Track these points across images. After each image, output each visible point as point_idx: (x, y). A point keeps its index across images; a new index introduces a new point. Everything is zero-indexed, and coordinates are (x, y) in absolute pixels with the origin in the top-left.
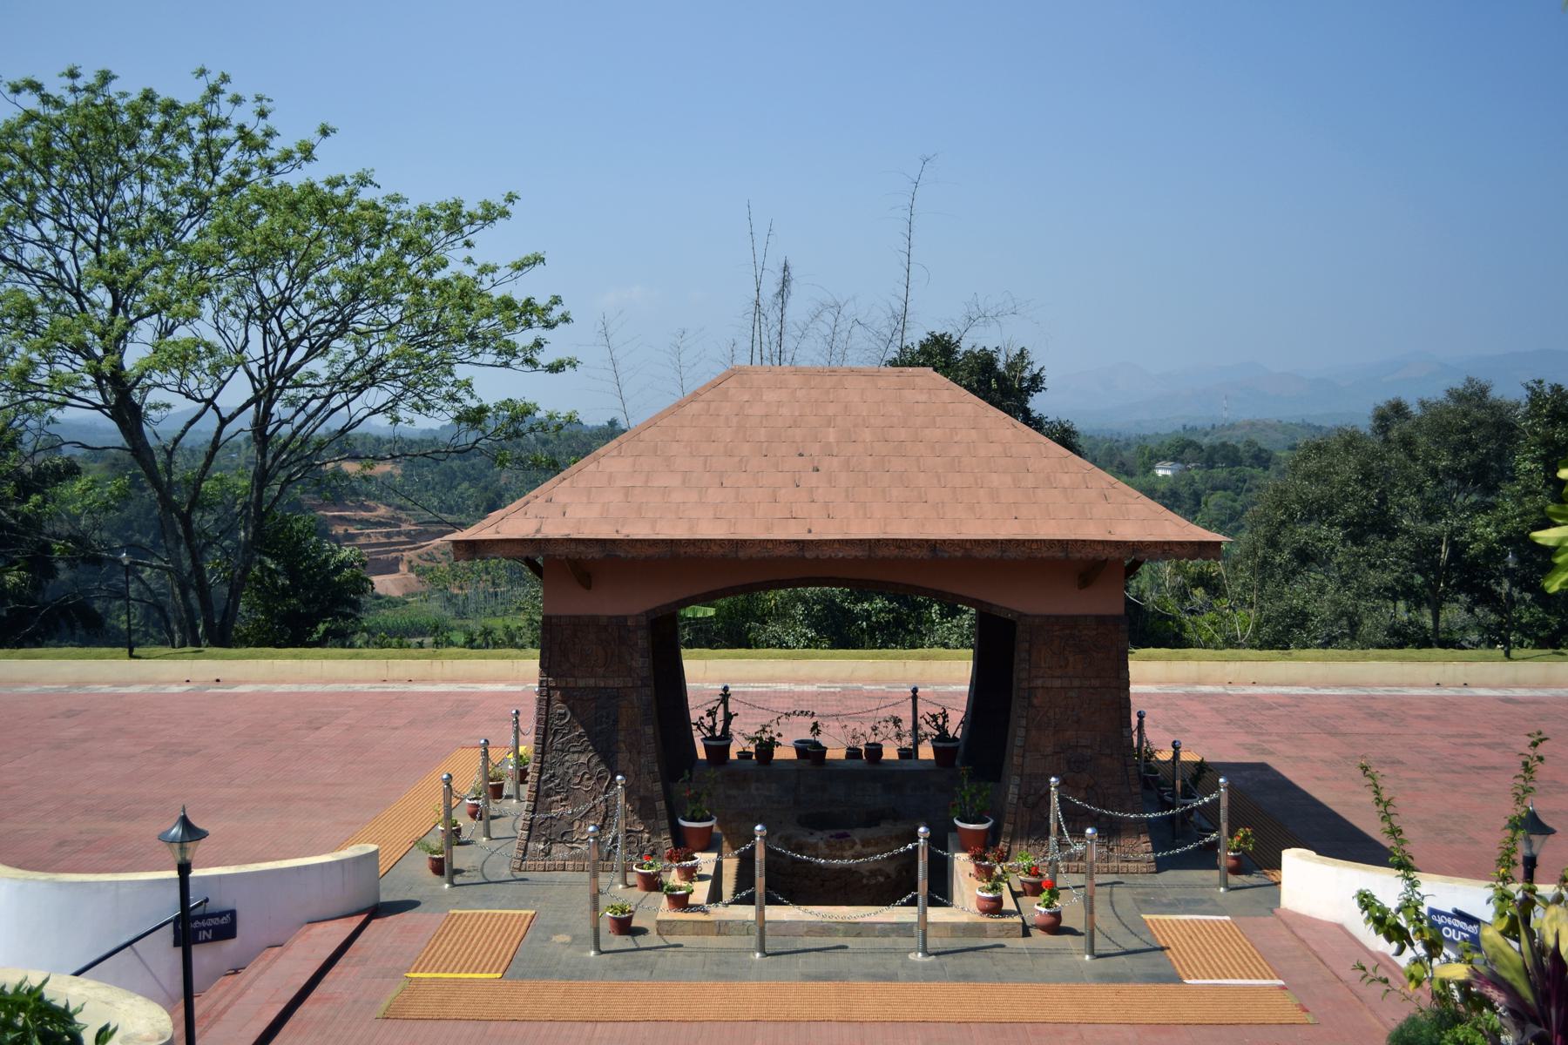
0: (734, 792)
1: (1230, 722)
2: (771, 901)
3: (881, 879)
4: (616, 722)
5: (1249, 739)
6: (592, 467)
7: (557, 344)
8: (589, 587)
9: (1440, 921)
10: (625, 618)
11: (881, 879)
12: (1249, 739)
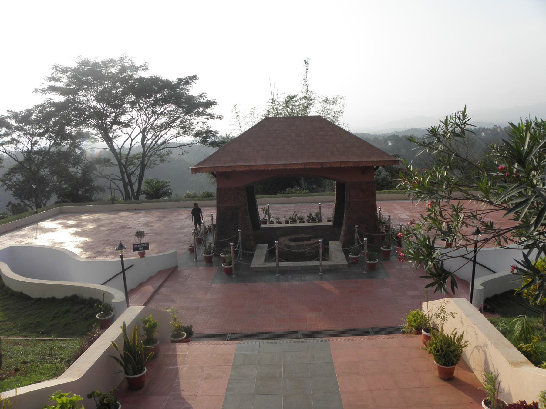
1: (405, 210)
2: (281, 261)
5: (410, 214)
7: (213, 110)
12: (410, 214)
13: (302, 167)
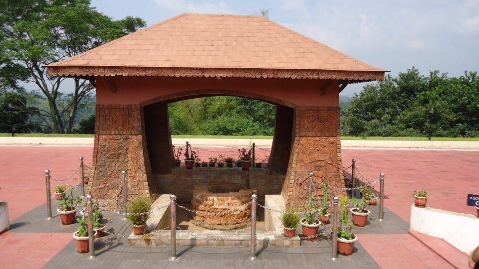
0: (188, 179)
3: (239, 212)
4: (127, 149)
6: (118, 43)
8: (116, 93)
9: (475, 199)
10: (131, 106)
11: (239, 212)
13: (229, 75)
